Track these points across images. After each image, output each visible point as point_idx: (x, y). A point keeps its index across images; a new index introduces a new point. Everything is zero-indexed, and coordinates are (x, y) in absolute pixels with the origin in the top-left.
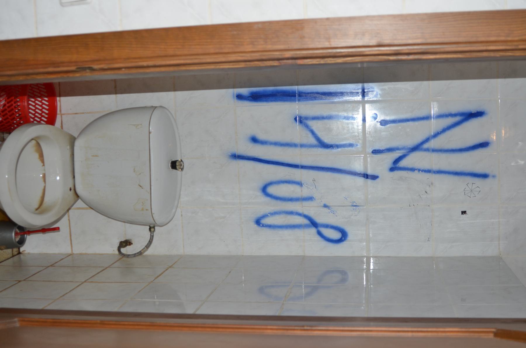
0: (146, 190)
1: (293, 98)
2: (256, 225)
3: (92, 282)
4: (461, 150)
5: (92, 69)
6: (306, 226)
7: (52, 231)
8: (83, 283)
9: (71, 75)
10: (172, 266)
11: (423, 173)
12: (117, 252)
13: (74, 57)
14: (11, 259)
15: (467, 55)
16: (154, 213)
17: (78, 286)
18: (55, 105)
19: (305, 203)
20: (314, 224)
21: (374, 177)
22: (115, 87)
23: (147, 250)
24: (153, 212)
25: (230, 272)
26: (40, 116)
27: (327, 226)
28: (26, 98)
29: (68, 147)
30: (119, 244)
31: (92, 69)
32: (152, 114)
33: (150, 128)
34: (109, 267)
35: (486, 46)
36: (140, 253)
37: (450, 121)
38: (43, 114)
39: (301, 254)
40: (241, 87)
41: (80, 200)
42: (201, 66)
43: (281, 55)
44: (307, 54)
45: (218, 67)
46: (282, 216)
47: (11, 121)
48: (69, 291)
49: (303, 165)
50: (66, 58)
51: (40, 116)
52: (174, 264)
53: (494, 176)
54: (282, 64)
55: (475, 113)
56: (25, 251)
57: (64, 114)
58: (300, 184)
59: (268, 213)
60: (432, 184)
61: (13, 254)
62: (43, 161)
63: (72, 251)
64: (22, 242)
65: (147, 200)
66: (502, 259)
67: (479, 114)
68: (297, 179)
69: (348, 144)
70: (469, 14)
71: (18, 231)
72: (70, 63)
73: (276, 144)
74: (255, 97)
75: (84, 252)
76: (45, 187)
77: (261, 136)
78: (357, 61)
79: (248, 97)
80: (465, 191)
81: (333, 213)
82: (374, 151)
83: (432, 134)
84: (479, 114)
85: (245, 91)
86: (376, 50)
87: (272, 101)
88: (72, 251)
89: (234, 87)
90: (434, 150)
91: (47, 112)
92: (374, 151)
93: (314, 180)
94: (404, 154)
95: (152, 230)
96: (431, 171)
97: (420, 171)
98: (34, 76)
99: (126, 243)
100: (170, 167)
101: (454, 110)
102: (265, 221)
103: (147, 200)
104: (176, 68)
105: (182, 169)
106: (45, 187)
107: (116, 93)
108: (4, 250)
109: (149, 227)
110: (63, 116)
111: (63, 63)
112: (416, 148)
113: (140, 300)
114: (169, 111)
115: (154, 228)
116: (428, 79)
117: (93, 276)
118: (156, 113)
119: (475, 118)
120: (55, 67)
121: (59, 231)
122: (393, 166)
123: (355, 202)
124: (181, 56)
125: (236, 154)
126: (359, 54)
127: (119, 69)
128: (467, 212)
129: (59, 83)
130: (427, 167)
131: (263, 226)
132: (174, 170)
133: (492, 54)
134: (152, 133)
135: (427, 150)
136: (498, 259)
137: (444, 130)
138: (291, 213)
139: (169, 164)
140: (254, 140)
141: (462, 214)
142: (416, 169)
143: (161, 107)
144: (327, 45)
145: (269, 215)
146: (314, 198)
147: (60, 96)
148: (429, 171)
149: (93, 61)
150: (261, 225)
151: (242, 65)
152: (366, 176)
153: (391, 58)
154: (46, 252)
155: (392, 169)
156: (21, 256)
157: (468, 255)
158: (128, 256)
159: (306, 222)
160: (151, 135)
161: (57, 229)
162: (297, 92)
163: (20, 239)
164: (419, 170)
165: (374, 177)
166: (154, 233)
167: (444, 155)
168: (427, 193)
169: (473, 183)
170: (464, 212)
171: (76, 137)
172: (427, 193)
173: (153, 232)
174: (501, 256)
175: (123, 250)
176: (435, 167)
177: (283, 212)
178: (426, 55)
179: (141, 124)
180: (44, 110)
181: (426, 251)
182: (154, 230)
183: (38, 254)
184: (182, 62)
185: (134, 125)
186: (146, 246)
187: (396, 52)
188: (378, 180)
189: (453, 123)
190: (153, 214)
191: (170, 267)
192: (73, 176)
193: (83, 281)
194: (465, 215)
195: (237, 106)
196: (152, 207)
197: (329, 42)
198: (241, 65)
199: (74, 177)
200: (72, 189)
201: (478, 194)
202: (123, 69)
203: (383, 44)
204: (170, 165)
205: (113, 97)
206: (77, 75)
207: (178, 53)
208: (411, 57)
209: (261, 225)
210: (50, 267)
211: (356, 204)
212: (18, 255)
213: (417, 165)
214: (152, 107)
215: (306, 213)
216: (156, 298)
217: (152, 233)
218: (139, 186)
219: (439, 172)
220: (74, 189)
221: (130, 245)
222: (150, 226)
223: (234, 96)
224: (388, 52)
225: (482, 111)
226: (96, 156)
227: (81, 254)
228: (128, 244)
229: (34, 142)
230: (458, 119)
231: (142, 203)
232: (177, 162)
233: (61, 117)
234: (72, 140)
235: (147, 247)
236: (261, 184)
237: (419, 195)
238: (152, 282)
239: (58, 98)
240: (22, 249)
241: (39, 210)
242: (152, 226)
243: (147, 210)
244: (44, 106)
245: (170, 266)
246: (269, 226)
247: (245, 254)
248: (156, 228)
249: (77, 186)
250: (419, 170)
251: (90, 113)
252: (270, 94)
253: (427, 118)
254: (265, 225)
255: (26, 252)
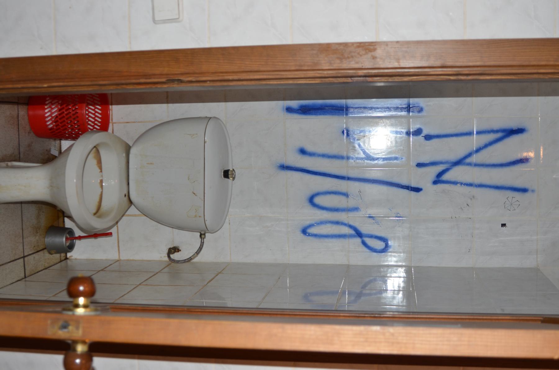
0: (200, 198)
1: (341, 112)
2: (302, 234)
3: (147, 285)
4: (502, 165)
5: (180, 81)
6: (351, 236)
7: (104, 236)
8: (138, 286)
9: (159, 86)
10: (221, 272)
11: (466, 187)
12: (166, 259)
13: (166, 70)
14: (60, 264)
15: (520, 77)
16: (206, 220)
17: (134, 288)
18: (108, 114)
19: (351, 214)
20: (359, 234)
21: (417, 190)
22: (167, 97)
23: (197, 256)
24: (206, 219)
25: (279, 278)
26: (93, 124)
27: (371, 236)
28: (85, 105)
29: (124, 155)
30: (168, 250)
31: (180, 81)
32: (207, 124)
33: (206, 138)
34: (159, 272)
35: (538, 69)
36: (190, 259)
37: (492, 137)
38: (96, 122)
39: (346, 263)
40: (291, 100)
41: (133, 206)
42: (280, 81)
43: (355, 73)
44: (378, 73)
45: (295, 82)
46: (329, 225)
47: (61, 128)
48: (126, 292)
49: (349, 177)
50: (158, 71)
51: (93, 124)
52: (222, 270)
53: (533, 191)
54: (354, 81)
55: (516, 130)
56: (72, 256)
57: (115, 123)
58: (346, 195)
59: (314, 223)
60: (473, 197)
61: (60, 259)
62: (101, 168)
63: (119, 257)
64: (71, 247)
65: (201, 207)
66: (539, 270)
67: (520, 131)
68: (344, 190)
69: (394, 157)
70: (522, 40)
71: (68, 237)
72: (161, 75)
73: (324, 156)
74: (305, 110)
75: (131, 258)
76: (102, 192)
77: (309, 148)
78: (422, 79)
79: (298, 110)
80: (505, 205)
81: (377, 223)
82: (418, 165)
83: (475, 149)
84: (520, 131)
85: (294, 104)
86: (439, 71)
87: (320, 114)
88: (119, 257)
89: (284, 99)
90: (476, 165)
91: (100, 120)
92: (418, 165)
93: (360, 192)
94: (446, 168)
95: (203, 236)
96: (473, 185)
97: (463, 185)
98: (124, 86)
99: (174, 250)
100: (223, 176)
101: (496, 127)
102: (311, 231)
103: (201, 207)
104: (257, 82)
105: (234, 178)
106: (102, 192)
107: (168, 102)
108: (54, 255)
109: (199, 234)
110: (114, 124)
111: (154, 75)
112: (458, 163)
113: (532, 169)
114: (222, 122)
115: (204, 234)
116: (472, 96)
117: (147, 280)
118: (211, 123)
119: (516, 135)
120: (146, 79)
121: (111, 237)
122: (436, 179)
123: (399, 213)
124: (264, 71)
125: (285, 165)
126: (424, 73)
127: (205, 81)
128: (506, 225)
129: (111, 94)
130: (469, 181)
131: (309, 235)
132: (226, 179)
133: (541, 76)
134: (207, 143)
135: (470, 164)
136: (536, 270)
137: (486, 146)
138: (337, 223)
139: (222, 172)
140: (303, 152)
141: (502, 226)
142: (459, 183)
143: (215, 117)
144: (396, 65)
145: (315, 224)
146: (359, 208)
147: (112, 105)
148: (470, 185)
149: (182, 74)
150: (307, 234)
151: (318, 81)
152: (410, 188)
153: (452, 78)
154: (92, 258)
155: (435, 183)
156: (68, 261)
157: (507, 266)
158: (178, 262)
159: (352, 232)
160: (206, 144)
161: (110, 234)
162: (345, 106)
163: (70, 244)
164: (461, 184)
165: (417, 190)
166: (205, 240)
167: (485, 170)
168: (468, 206)
169: (513, 197)
170: (503, 225)
171: (131, 145)
172: (468, 206)
173: (204, 238)
174: (538, 268)
175: (172, 256)
176: (477, 181)
177: (329, 222)
178: (482, 76)
179: (197, 134)
180: (96, 118)
181: (466, 262)
182: (205, 237)
183: (85, 259)
184: (265, 77)
185: (190, 135)
186: (196, 252)
187: (457, 73)
188: (421, 193)
189: (495, 139)
190: (205, 220)
191: (220, 273)
192: (127, 183)
193: (138, 284)
194: (504, 227)
195: (286, 119)
196: (205, 214)
197: (398, 62)
198: (317, 81)
199: (128, 184)
200: (127, 195)
201: (517, 208)
202: (208, 82)
203: (446, 66)
204: (222, 174)
205: (164, 106)
206: (165, 86)
207: (262, 69)
208: (470, 78)
209: (307, 234)
210: (101, 272)
211: (400, 215)
212: (66, 260)
213: (460, 179)
214: (206, 117)
215: (352, 223)
216: (204, 302)
217: (202, 239)
218: (193, 194)
219: (481, 186)
220: (128, 196)
221: (178, 252)
222: (200, 233)
223: (283, 108)
224: (450, 73)
225: (523, 128)
226: (151, 164)
227: (128, 260)
228: (177, 250)
229: (95, 149)
230: (499, 135)
231: (196, 209)
232: (230, 171)
233: (113, 125)
234: (128, 149)
235: (197, 253)
236: (309, 193)
237: (461, 208)
238: (205, 285)
239: (110, 106)
240: (69, 255)
241: (98, 214)
242: (203, 233)
243: (200, 217)
244: (97, 114)
245: (219, 272)
246: (315, 236)
247: (291, 262)
248: (206, 234)
249: (131, 193)
250: (461, 184)
251: (141, 122)
252: (319, 108)
253: (470, 134)
254: (311, 234)
255: (73, 258)
